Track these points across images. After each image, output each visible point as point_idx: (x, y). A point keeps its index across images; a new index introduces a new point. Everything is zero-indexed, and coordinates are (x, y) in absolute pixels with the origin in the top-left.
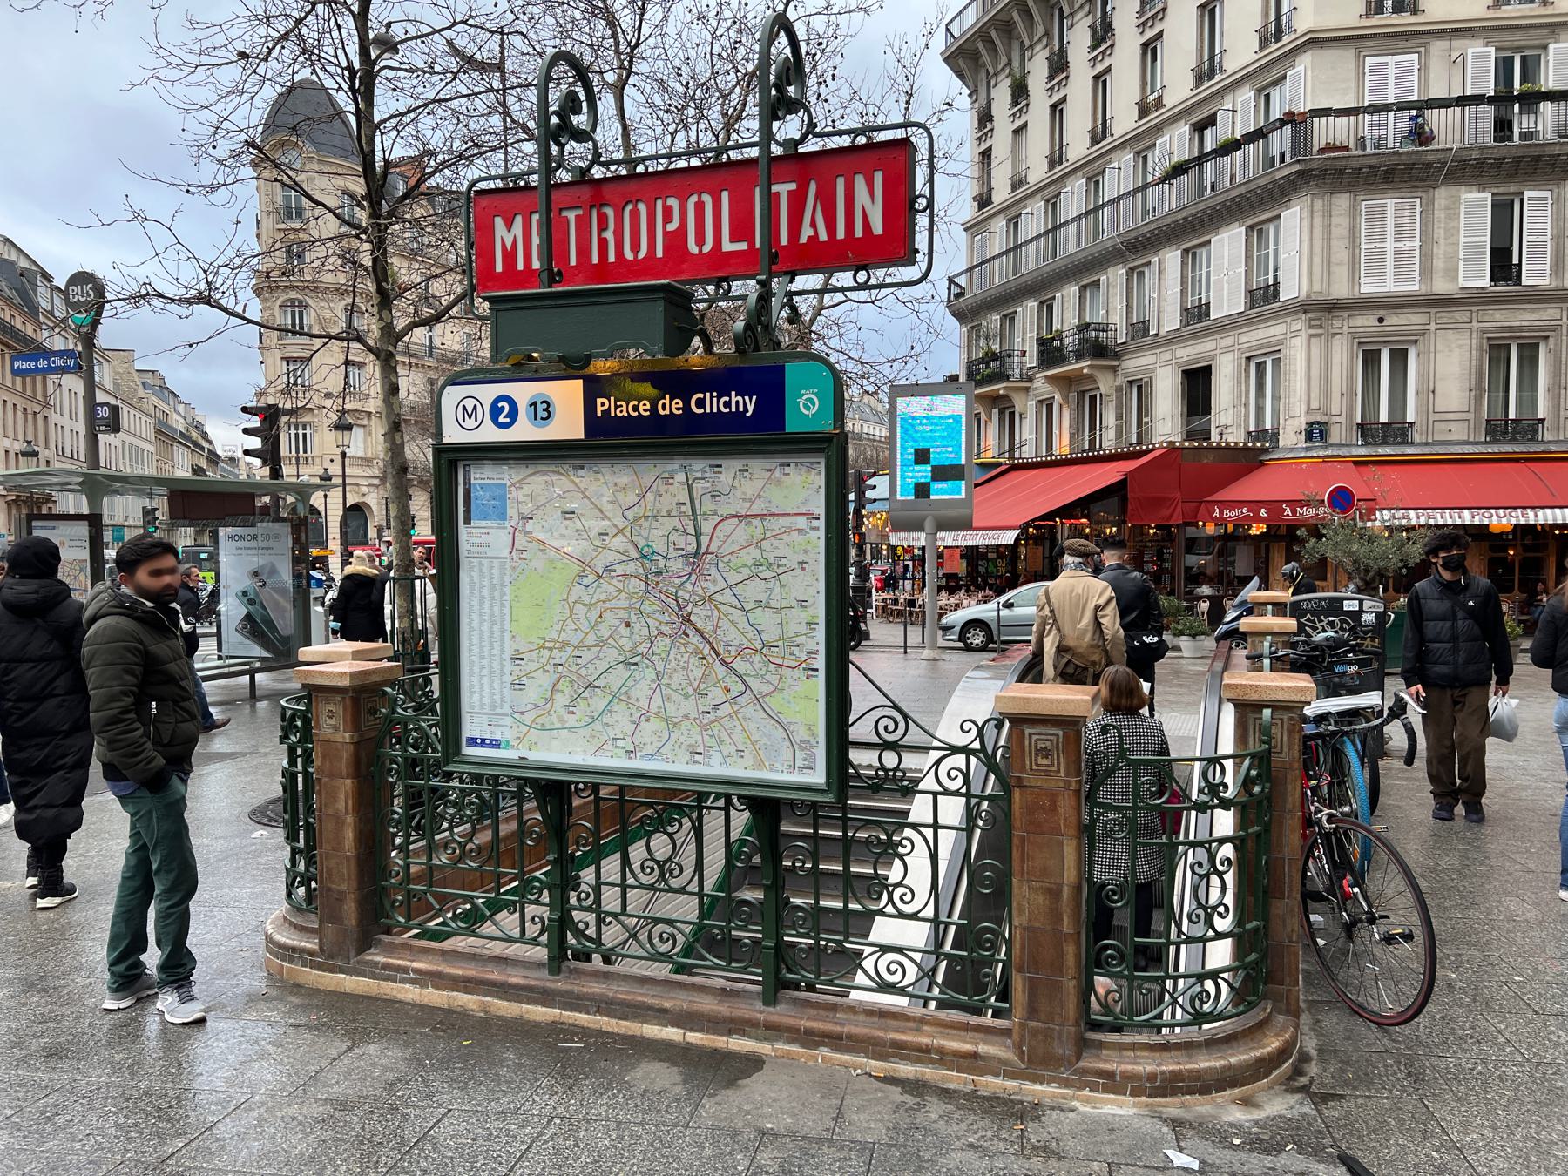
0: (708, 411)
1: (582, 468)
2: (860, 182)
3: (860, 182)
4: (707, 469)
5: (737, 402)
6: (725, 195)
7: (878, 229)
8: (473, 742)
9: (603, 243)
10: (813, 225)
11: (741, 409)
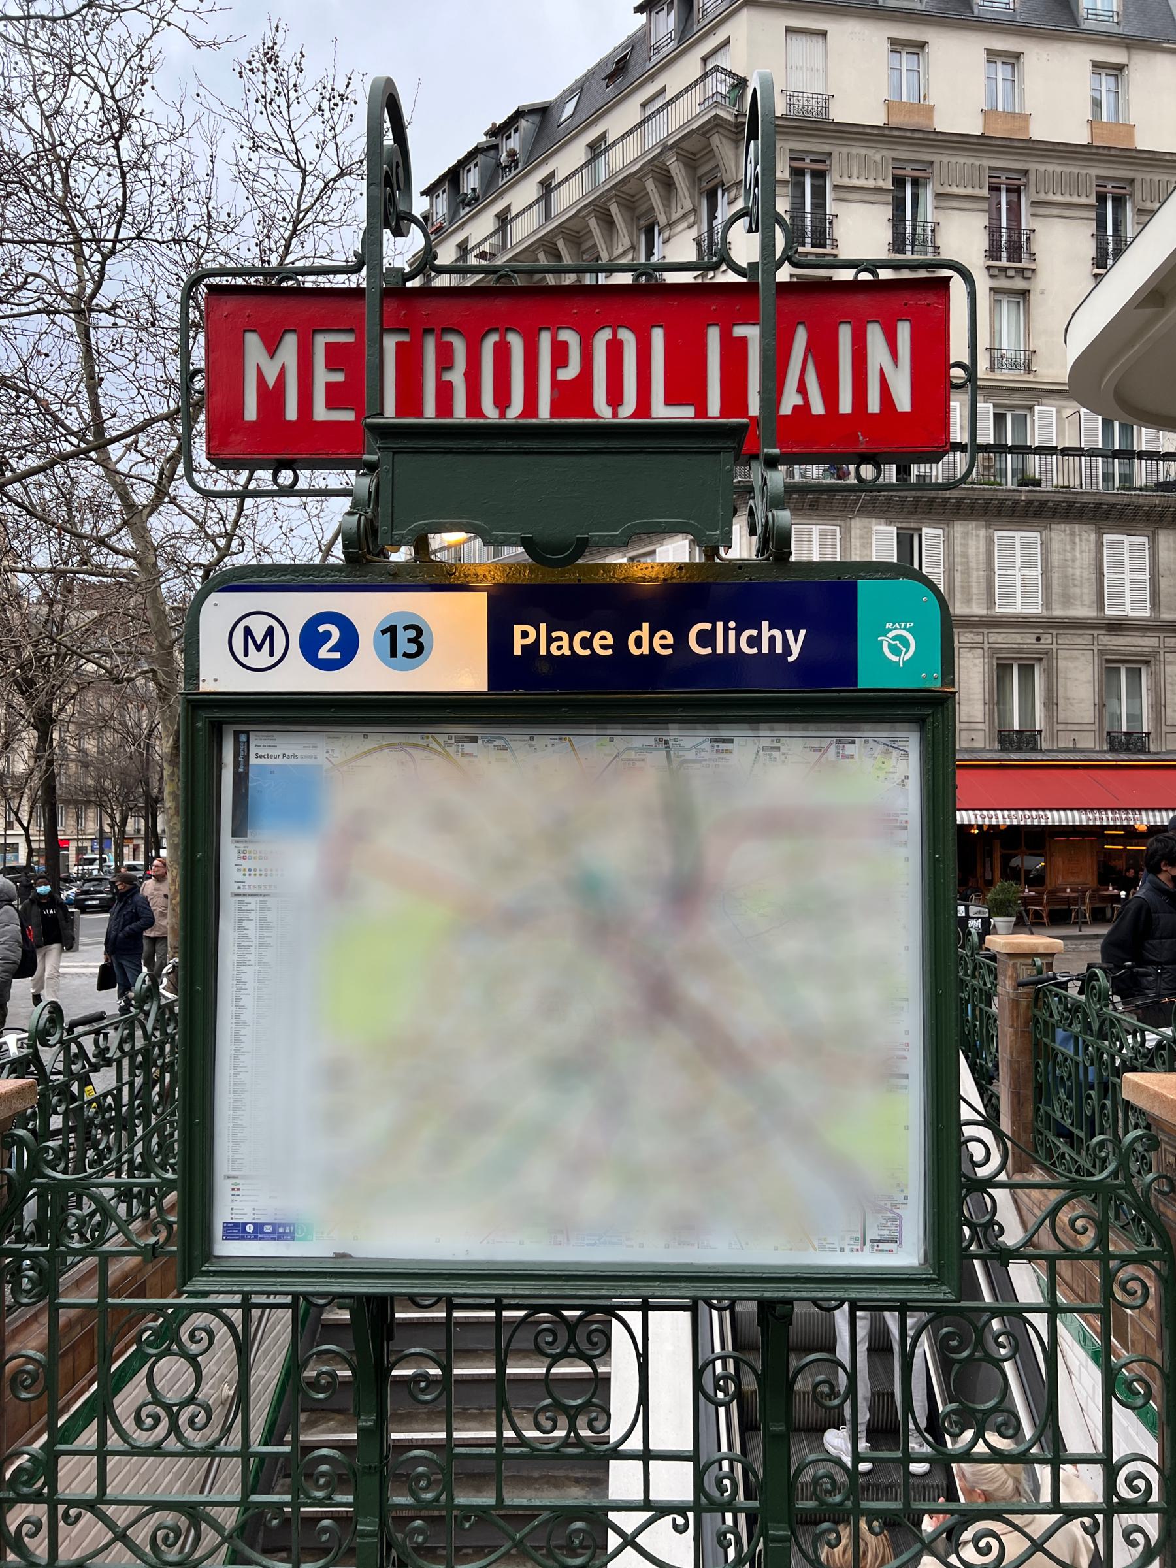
0: (720, 650)
1: (474, 740)
2: (875, 335)
3: (875, 335)
4: (707, 745)
5: (772, 639)
6: (658, 336)
7: (903, 402)
8: (236, 1231)
9: (445, 392)
10: (802, 389)
11: (779, 649)
